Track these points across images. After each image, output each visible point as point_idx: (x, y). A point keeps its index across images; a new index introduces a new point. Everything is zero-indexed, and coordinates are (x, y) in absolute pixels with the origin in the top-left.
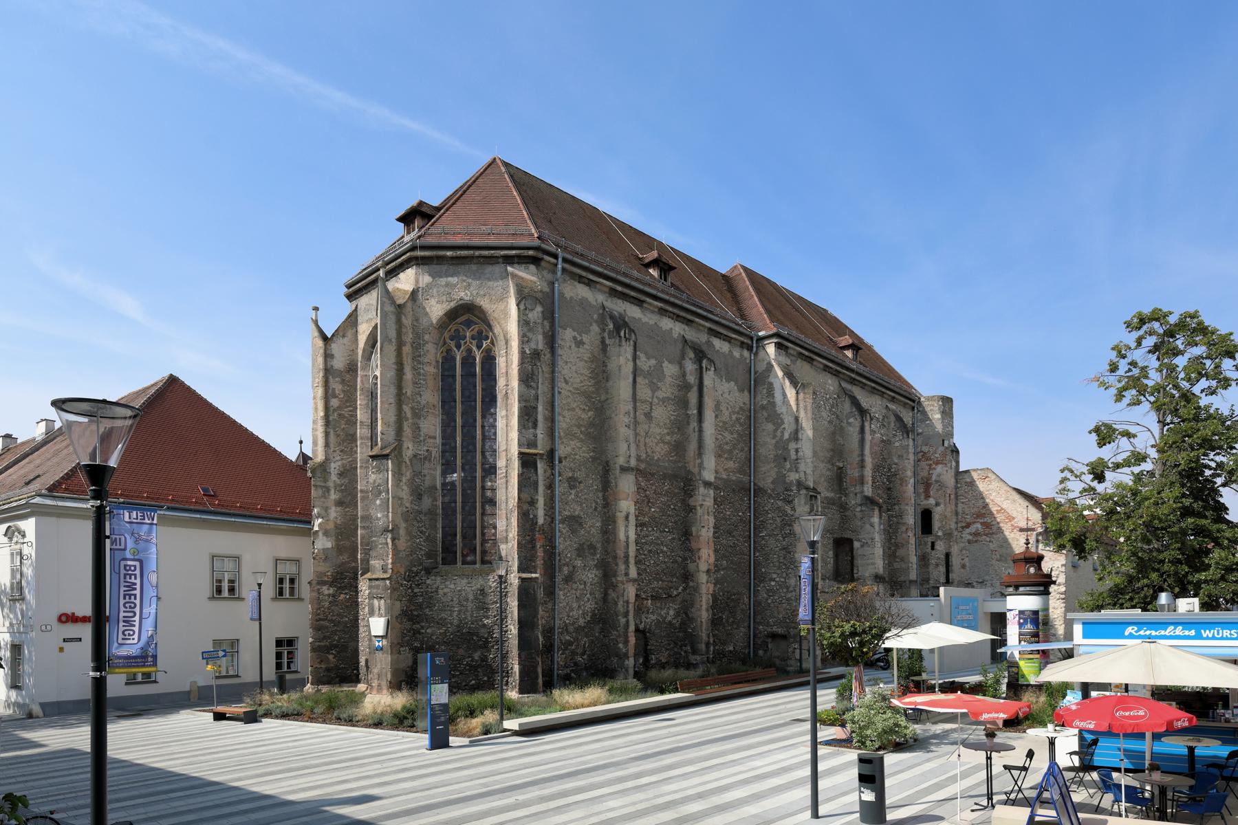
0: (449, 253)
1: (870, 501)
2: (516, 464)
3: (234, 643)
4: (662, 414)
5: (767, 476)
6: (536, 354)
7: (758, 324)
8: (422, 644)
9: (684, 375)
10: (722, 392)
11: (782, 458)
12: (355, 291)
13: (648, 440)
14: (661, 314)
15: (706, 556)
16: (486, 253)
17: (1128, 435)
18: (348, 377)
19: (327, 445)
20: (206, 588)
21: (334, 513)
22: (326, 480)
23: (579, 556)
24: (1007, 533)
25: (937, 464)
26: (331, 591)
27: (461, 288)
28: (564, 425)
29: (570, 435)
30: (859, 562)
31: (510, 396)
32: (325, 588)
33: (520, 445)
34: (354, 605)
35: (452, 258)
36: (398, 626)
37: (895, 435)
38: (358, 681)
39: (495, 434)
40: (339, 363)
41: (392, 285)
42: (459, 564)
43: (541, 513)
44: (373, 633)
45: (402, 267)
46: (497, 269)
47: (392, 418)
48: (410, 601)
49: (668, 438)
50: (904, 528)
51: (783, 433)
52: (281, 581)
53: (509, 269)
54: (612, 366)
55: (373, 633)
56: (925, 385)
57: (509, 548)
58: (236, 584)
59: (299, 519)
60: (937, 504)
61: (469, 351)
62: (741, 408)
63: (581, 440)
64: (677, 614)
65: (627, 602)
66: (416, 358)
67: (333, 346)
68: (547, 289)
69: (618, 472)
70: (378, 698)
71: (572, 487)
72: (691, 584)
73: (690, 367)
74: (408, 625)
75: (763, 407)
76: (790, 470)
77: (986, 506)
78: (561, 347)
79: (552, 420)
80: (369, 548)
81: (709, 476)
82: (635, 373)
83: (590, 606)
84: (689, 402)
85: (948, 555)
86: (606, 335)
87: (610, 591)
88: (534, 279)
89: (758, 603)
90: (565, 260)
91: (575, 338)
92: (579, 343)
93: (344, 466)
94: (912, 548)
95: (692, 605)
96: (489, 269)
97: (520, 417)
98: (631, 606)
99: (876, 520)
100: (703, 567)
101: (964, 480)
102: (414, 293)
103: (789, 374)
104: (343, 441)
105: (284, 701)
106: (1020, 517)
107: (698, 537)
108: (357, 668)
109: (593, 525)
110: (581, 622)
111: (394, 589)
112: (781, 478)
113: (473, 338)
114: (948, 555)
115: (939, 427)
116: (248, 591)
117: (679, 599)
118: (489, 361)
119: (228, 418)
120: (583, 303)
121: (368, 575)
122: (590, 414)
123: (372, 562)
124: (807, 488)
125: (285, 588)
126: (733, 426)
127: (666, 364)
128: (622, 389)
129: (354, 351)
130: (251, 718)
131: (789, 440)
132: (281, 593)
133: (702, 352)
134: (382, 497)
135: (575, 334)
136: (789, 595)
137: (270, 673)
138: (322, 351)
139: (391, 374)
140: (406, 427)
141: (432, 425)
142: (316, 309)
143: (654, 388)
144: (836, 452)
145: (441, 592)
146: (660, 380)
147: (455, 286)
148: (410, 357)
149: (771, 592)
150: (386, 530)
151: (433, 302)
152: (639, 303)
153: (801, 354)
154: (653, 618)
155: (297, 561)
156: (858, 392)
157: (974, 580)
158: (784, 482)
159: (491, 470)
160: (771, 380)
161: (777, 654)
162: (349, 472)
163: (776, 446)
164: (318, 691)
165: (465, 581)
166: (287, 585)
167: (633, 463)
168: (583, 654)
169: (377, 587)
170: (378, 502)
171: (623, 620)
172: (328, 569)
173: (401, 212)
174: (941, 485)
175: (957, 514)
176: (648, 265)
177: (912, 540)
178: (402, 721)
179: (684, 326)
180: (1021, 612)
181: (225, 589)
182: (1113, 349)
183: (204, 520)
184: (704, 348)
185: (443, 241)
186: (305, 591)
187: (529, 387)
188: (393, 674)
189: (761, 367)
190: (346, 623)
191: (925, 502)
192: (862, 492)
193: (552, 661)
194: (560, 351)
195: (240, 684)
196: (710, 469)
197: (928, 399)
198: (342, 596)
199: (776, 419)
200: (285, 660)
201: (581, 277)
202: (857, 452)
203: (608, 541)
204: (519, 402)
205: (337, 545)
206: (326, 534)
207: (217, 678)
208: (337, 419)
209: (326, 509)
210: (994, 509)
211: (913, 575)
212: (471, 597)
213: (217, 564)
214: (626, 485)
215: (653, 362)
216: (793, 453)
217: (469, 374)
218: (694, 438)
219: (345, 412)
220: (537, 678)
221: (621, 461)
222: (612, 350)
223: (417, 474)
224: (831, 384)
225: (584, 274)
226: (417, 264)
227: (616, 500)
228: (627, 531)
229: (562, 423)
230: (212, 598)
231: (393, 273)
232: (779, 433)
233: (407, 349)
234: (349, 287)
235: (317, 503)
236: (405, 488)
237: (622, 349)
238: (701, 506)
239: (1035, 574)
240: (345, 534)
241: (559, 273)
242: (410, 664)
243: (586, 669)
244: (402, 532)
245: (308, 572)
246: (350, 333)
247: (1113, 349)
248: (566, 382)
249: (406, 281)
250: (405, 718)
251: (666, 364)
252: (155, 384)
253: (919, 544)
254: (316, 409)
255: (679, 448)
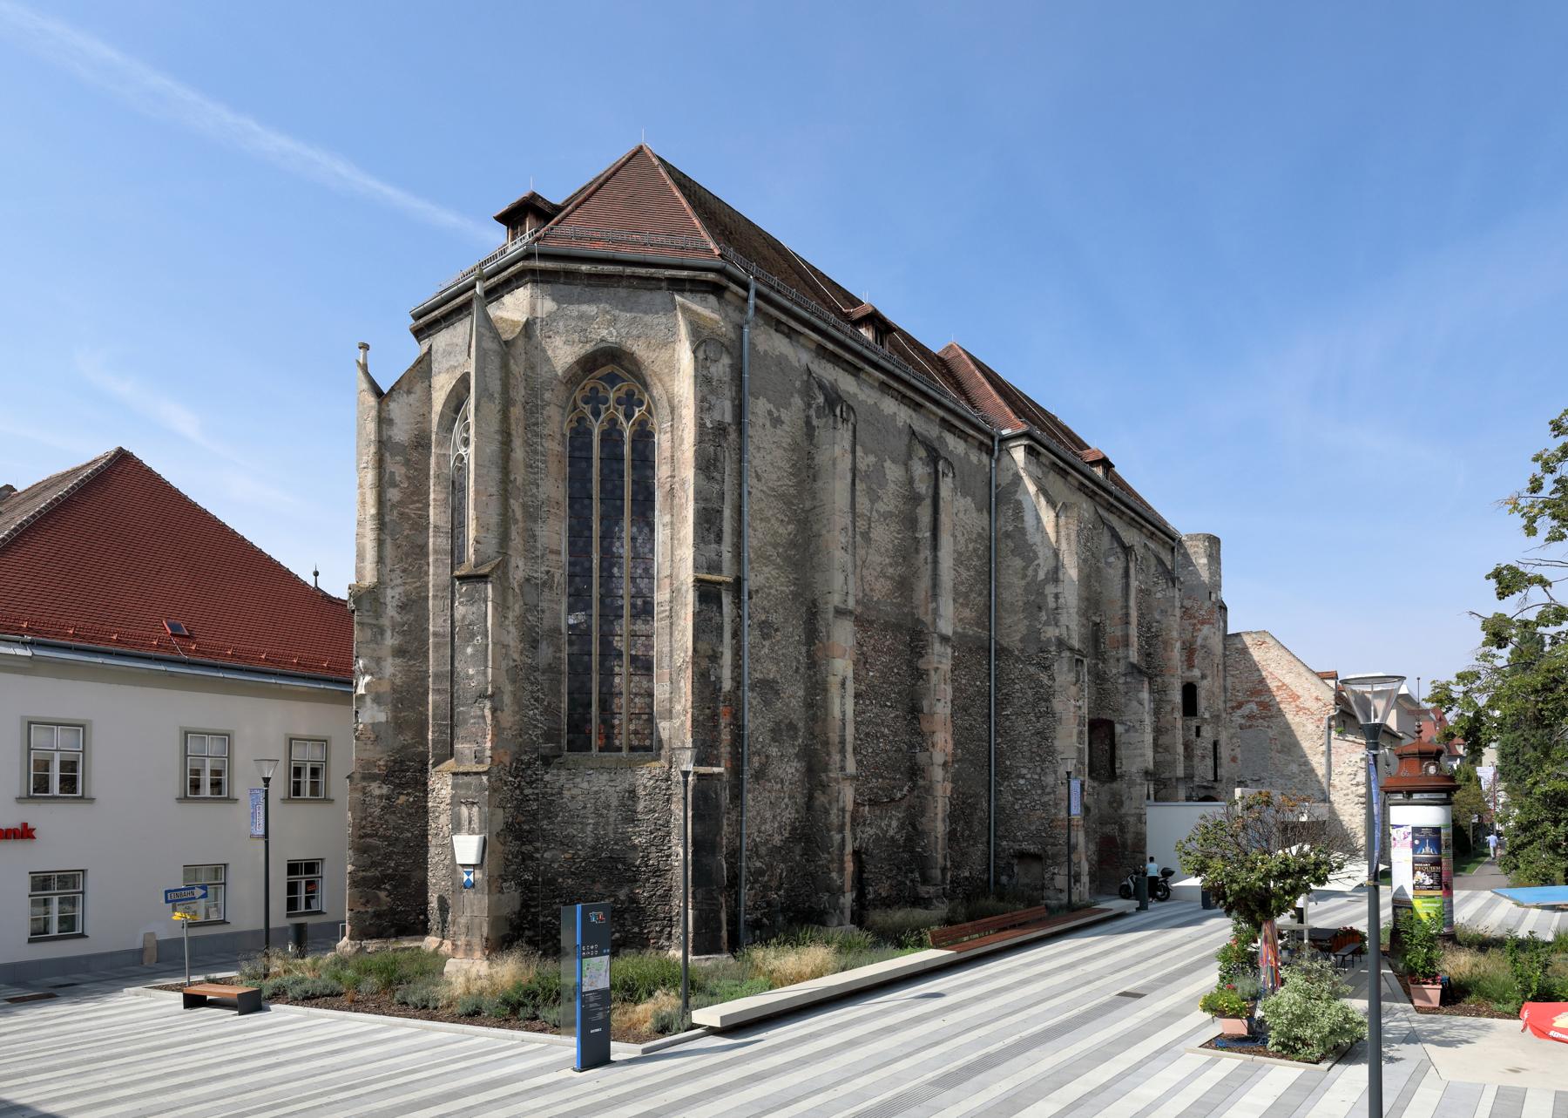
0: (584, 268)
1: (1134, 670)
2: (690, 597)
3: (219, 870)
4: (884, 535)
5: (1014, 630)
6: (721, 429)
7: (998, 419)
8: (536, 876)
9: (911, 481)
10: (960, 514)
11: (1035, 606)
12: (428, 324)
13: (865, 572)
14: (883, 391)
15: (942, 743)
16: (642, 271)
17: (1543, 582)
18: (415, 456)
19: (380, 560)
20: (174, 783)
21: (390, 667)
22: (378, 615)
23: (774, 740)
24: (1289, 717)
25: (1203, 623)
26: (385, 790)
27: (605, 322)
28: (755, 543)
29: (765, 559)
30: (1122, 752)
31: (679, 493)
32: (374, 785)
33: (696, 568)
34: (421, 812)
35: (590, 275)
36: (501, 848)
37: (1156, 584)
38: (424, 931)
39: (652, 550)
40: (401, 433)
41: (494, 311)
42: (595, 751)
43: (727, 673)
44: (459, 861)
45: (508, 285)
46: (659, 297)
47: (493, 518)
48: (517, 808)
49: (891, 570)
50: (1169, 708)
51: (1036, 571)
52: (298, 772)
53: (678, 298)
54: (822, 458)
55: (459, 861)
56: (1181, 521)
57: (677, 724)
58: (225, 778)
59: (334, 678)
60: (1204, 677)
61: (613, 421)
62: (979, 535)
63: (779, 567)
64: (901, 827)
65: (843, 810)
66: (531, 427)
67: (392, 405)
68: (733, 336)
69: (831, 616)
70: (468, 968)
71: (765, 636)
72: (921, 782)
73: (920, 470)
74: (514, 846)
75: (1008, 535)
76: (1047, 623)
77: (1262, 681)
78: (753, 425)
79: (739, 533)
80: (451, 723)
81: (946, 627)
82: (854, 470)
83: (788, 815)
84: (918, 521)
85: (1215, 744)
86: (812, 412)
87: (818, 794)
88: (715, 316)
89: (1000, 809)
90: (759, 295)
91: (770, 413)
92: (776, 422)
93: (407, 594)
94: (1179, 733)
95: (923, 813)
96: (645, 297)
97: (697, 524)
98: (848, 816)
99: (1145, 695)
100: (939, 758)
101: (1233, 643)
102: (528, 326)
103: (1042, 490)
104: (407, 555)
105: (308, 969)
106: (1306, 695)
107: (932, 714)
108: (425, 912)
109: (793, 694)
110: (777, 840)
111: (494, 790)
112: (1033, 635)
113: (619, 401)
114: (1215, 744)
115: (1205, 575)
116: (243, 783)
117: (904, 804)
118: (644, 437)
119: (213, 520)
120: (781, 361)
121: (450, 764)
122: (791, 527)
123: (458, 746)
124: (1071, 649)
125: (305, 782)
126: (969, 559)
127: (888, 464)
128: (837, 492)
129: (425, 417)
130: (251, 1004)
131: (1046, 581)
132: (297, 792)
133: (935, 450)
134: (477, 646)
135: (771, 407)
136: (1046, 799)
137: (279, 918)
138: (374, 413)
139: (493, 448)
140: (514, 535)
141: (554, 533)
142: (365, 347)
143: (874, 498)
144: (1092, 602)
145: (566, 794)
146: (881, 486)
147: (593, 318)
148: (521, 424)
149: (1018, 793)
150: (483, 696)
151: (558, 341)
152: (855, 371)
153: (1054, 463)
154: (871, 832)
155: (324, 742)
156: (1114, 520)
157: (1247, 776)
158: (1039, 640)
159: (645, 610)
160: (1019, 496)
161: (1027, 881)
162: (414, 604)
163: (1027, 589)
164: (362, 949)
165: (605, 777)
166: (306, 779)
167: (851, 604)
168: (779, 888)
169: (468, 786)
170: (469, 650)
171: (837, 837)
172: (380, 757)
173: (504, 207)
174: (1209, 653)
175: (1225, 689)
176: (858, 323)
177: (1179, 724)
178: (518, 1009)
179: (910, 412)
180: (1416, 830)
181: (205, 785)
182: (1536, 460)
183: (172, 674)
184: (936, 444)
185: (576, 248)
186: (338, 784)
187: (710, 478)
188: (492, 926)
189: (1005, 479)
190: (408, 841)
191: (1188, 674)
192: (1127, 657)
193: (737, 901)
194: (750, 431)
195: (228, 935)
196: (948, 618)
197: (1191, 537)
198: (402, 799)
199: (1026, 552)
200: (302, 895)
201: (779, 322)
202: (1120, 603)
203: (814, 718)
204: (696, 500)
205: (396, 718)
206: (378, 699)
207: (191, 925)
208: (397, 523)
209: (378, 660)
210: (1272, 684)
211: (1180, 772)
212: (614, 802)
213: (193, 745)
214: (843, 635)
215: (872, 459)
216: (1051, 600)
217: (612, 457)
218: (926, 572)
219: (411, 510)
220: (719, 929)
221: (836, 599)
222: (822, 435)
223: (531, 608)
224: (1085, 507)
225: (784, 318)
226: (535, 282)
227: (829, 657)
228: (843, 704)
229: (752, 540)
230: (184, 799)
231: (494, 294)
232: (1030, 572)
233: (516, 412)
234: (417, 317)
235: (363, 651)
236: (512, 629)
237: (838, 435)
238: (936, 669)
239: (1437, 775)
240: (406, 700)
241: (751, 312)
242: (517, 908)
243: (783, 911)
244: (507, 699)
245: (345, 760)
246: (419, 389)
247: (1536, 460)
248: (759, 478)
249: (515, 307)
250: (521, 1004)
251: (888, 464)
252: (95, 461)
253: (1186, 729)
254: (363, 503)
255: (904, 586)
